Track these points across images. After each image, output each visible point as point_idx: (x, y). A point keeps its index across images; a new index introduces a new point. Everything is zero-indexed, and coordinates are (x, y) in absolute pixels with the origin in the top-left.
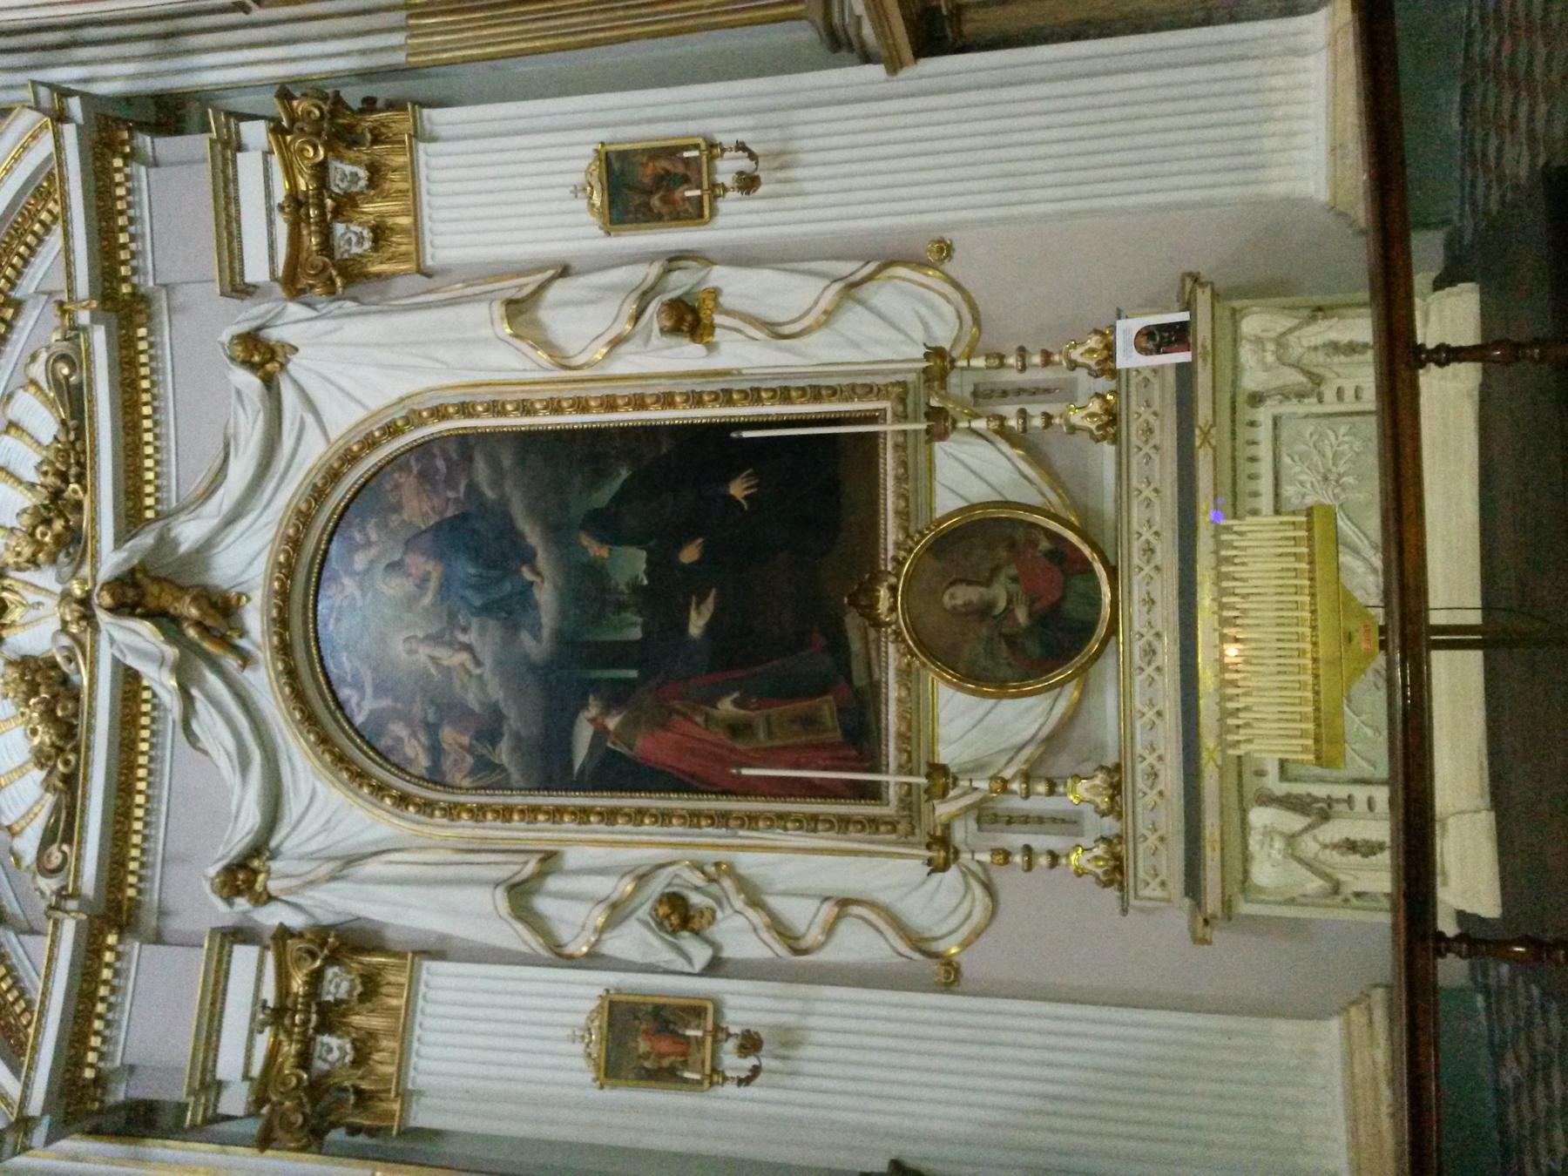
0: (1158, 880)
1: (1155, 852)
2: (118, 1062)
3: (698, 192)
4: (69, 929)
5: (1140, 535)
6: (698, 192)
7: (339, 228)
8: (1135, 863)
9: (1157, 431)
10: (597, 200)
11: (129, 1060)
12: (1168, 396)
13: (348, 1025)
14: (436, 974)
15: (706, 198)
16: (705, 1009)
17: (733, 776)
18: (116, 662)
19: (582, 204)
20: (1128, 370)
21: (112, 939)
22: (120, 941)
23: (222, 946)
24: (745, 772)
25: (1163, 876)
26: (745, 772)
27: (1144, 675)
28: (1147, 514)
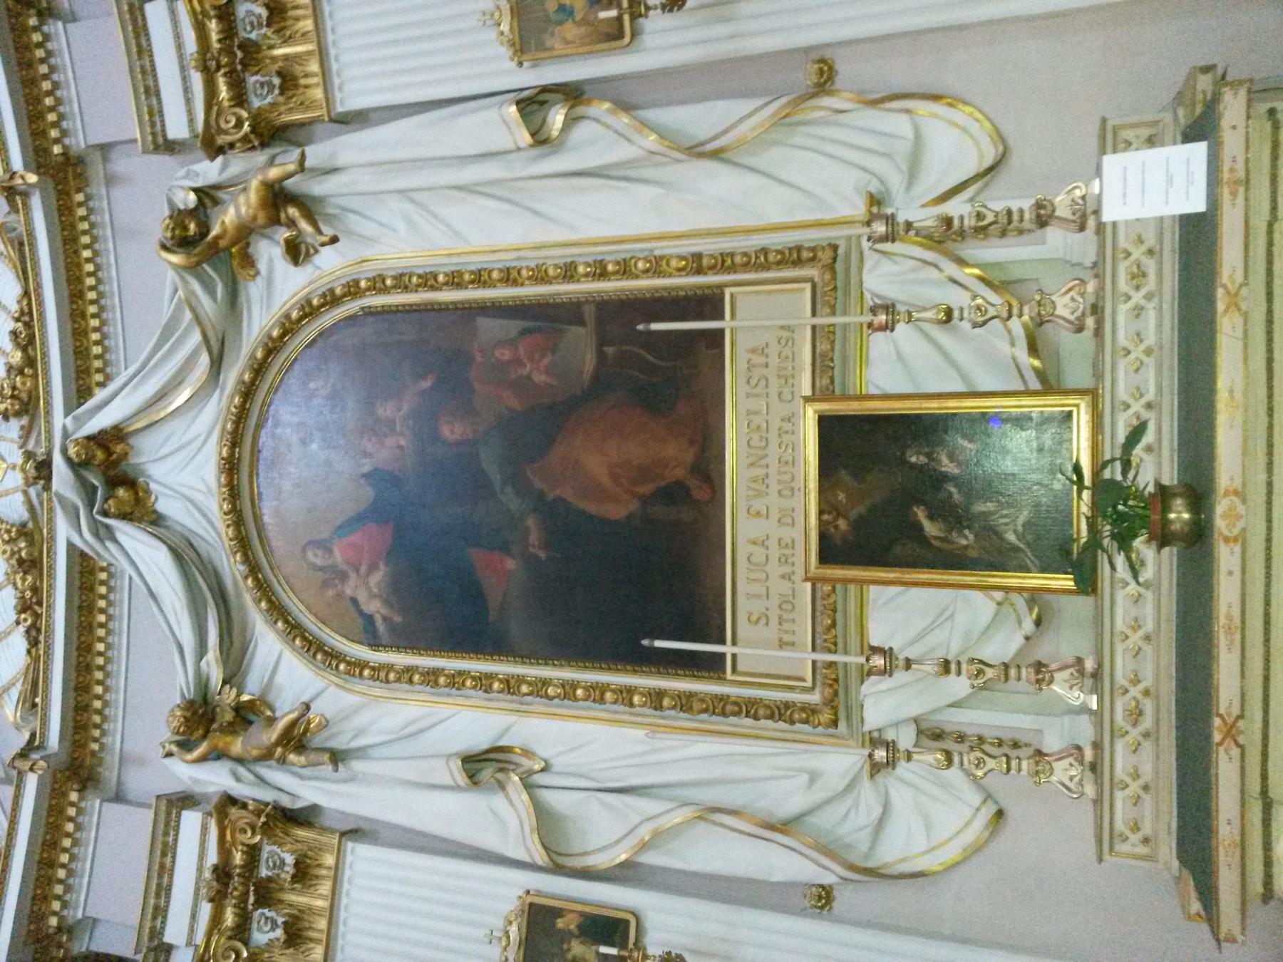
0: (1141, 633)
1: (1137, 801)
2: (80, 915)
3: (613, 13)
4: (32, 781)
5: (1129, 254)
6: (613, 13)
7: (252, 80)
8: (1112, 806)
9: (1152, 277)
10: (505, 27)
11: (91, 912)
12: (1167, 323)
13: (281, 901)
14: (360, 856)
15: (626, 18)
16: (627, 922)
17: (641, 332)
18: (71, 546)
19: (492, 34)
20: (1114, 224)
21: (74, 796)
22: (81, 799)
23: (168, 814)
24: (655, 326)
25: (1147, 829)
26: (655, 326)
27: (1131, 304)
28: (1133, 612)
